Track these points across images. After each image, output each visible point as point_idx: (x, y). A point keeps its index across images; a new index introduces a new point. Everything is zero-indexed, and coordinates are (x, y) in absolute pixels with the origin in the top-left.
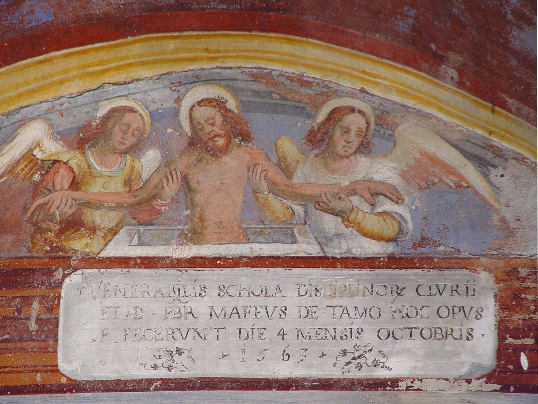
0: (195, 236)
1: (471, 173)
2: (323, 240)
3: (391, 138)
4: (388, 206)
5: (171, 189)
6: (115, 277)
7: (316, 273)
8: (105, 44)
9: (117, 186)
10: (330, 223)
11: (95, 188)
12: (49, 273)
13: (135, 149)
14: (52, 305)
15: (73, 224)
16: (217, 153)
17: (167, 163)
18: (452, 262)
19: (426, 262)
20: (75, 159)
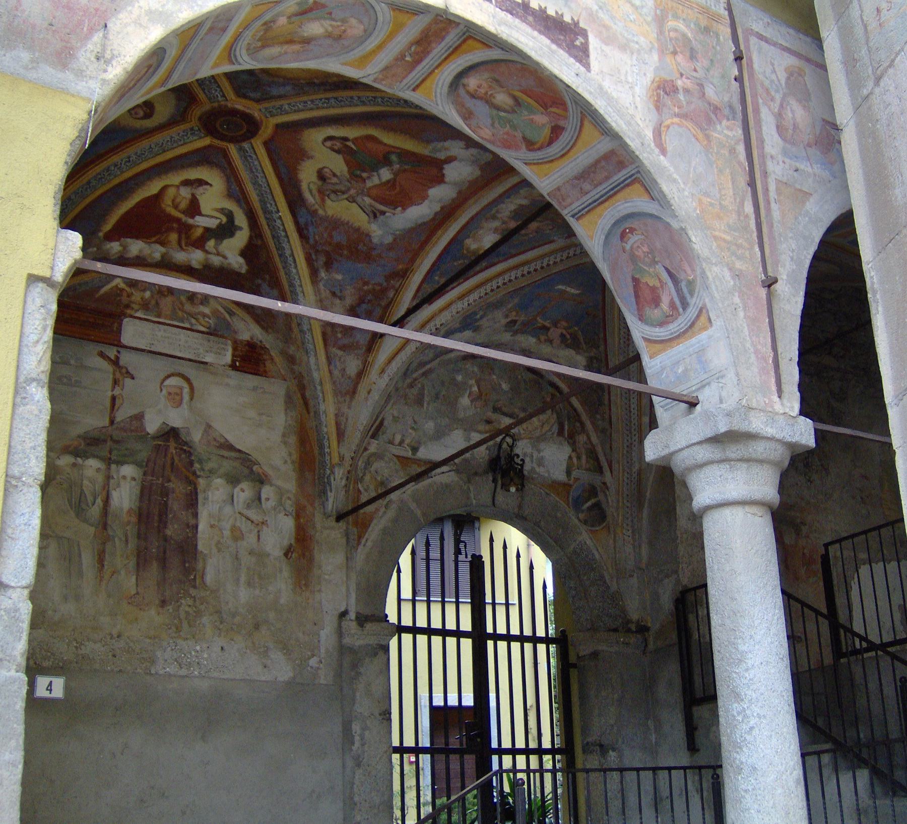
0: (159, 316)
1: (227, 316)
2: (191, 324)
3: (208, 302)
4: (207, 319)
5: (153, 302)
6: (137, 321)
7: (189, 332)
8: (282, 273)
9: (139, 299)
10: (193, 321)
11: (133, 298)
12: (120, 316)
13: (144, 290)
14: (120, 325)
15: (128, 306)
16: (165, 296)
17: (152, 296)
18: (222, 336)
19: (216, 335)
20: (128, 289)
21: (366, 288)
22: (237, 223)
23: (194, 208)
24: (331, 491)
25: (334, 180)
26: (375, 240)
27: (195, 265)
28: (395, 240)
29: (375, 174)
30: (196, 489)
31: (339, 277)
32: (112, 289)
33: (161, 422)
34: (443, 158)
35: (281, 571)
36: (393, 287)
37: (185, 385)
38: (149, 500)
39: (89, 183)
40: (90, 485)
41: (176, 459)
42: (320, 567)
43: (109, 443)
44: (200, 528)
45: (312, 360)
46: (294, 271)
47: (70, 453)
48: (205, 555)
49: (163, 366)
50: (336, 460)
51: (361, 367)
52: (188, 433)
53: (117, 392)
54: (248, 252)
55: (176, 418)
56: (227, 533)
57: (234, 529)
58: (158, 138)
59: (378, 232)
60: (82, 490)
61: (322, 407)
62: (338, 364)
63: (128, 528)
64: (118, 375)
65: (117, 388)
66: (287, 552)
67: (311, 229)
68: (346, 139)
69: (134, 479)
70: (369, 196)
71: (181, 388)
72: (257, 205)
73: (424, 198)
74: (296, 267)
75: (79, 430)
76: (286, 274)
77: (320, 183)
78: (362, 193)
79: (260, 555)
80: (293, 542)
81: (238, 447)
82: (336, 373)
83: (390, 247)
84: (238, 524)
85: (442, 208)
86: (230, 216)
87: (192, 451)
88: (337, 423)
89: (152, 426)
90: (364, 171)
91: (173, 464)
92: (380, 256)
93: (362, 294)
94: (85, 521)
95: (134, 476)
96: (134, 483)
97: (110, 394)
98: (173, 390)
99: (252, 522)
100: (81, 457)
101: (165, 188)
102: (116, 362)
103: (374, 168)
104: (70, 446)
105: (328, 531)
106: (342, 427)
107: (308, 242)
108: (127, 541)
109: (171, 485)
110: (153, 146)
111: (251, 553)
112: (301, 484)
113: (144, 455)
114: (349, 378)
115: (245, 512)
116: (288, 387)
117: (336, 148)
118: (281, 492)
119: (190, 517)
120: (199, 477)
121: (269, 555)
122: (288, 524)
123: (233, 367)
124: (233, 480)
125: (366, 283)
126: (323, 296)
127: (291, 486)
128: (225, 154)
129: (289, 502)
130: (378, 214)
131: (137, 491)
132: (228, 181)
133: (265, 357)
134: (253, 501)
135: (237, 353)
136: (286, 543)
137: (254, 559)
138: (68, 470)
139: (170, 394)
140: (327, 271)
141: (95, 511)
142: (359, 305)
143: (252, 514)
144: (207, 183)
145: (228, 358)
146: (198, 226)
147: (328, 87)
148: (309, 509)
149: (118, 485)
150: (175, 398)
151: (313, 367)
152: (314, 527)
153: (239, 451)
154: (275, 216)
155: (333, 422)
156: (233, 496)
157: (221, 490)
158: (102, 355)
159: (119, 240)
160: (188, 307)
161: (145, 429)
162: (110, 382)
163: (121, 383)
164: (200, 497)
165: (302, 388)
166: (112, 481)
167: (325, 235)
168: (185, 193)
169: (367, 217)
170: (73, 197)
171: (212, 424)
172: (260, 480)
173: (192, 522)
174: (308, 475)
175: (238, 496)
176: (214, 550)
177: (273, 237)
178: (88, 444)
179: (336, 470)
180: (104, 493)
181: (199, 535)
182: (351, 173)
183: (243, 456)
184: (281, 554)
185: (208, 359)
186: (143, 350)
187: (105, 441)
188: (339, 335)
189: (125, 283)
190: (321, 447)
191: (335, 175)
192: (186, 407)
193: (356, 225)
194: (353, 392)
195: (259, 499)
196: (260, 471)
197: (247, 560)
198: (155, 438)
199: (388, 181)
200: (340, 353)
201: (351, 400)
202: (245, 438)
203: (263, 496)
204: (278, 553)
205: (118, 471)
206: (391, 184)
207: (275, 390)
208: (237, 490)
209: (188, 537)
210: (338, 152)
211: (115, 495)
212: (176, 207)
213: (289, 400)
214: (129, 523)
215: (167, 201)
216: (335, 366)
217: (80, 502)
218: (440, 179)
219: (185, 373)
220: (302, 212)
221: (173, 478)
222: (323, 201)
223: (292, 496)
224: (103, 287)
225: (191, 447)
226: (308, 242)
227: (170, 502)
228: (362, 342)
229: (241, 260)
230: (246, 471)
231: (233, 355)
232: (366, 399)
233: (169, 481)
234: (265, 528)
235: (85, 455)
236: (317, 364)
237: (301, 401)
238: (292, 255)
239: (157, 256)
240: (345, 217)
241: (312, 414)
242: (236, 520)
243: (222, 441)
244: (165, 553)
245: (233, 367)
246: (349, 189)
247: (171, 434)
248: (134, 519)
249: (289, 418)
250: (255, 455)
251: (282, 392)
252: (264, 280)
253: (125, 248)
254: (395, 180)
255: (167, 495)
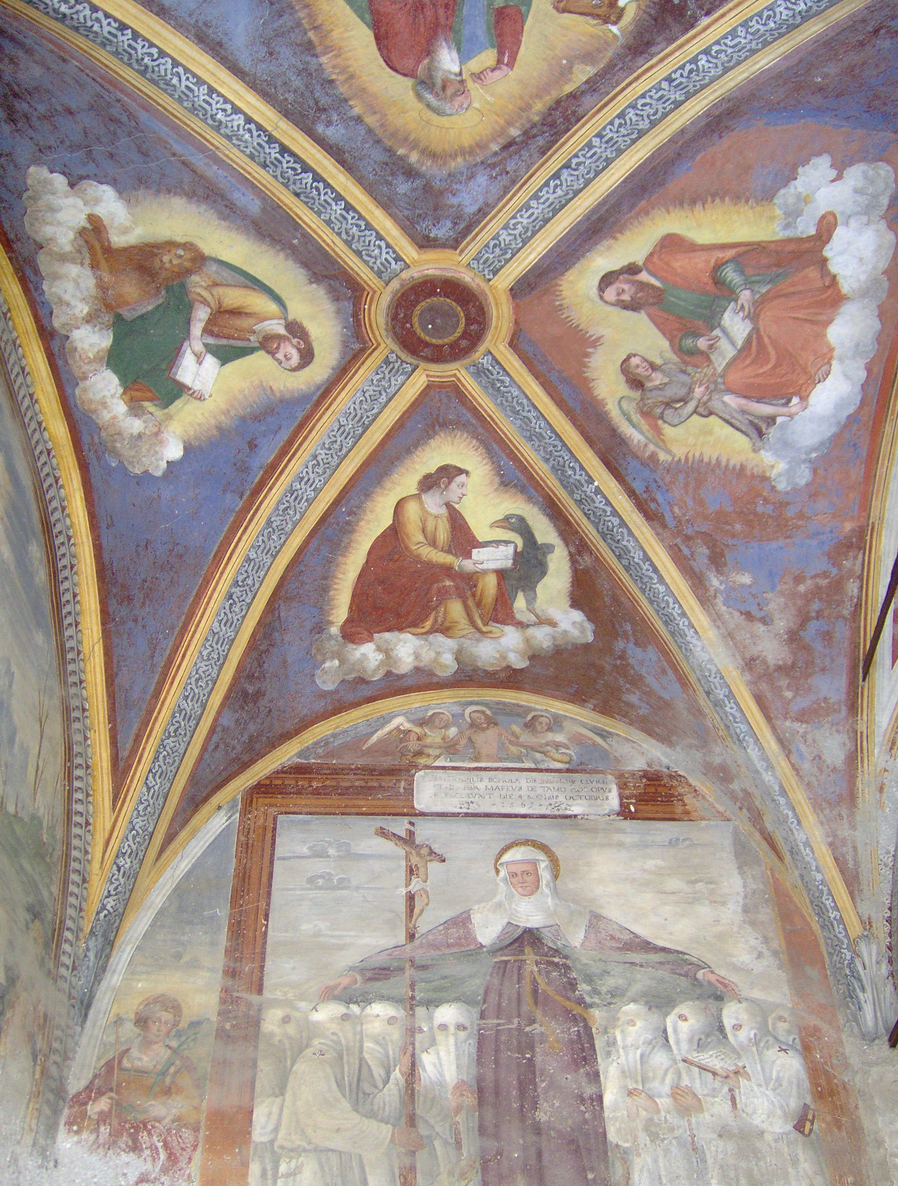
0: (477, 759)
1: (599, 740)
2: (536, 762)
5: (463, 742)
6: (440, 772)
7: (534, 774)
9: (438, 740)
10: (538, 756)
11: (429, 741)
12: (409, 771)
13: (446, 727)
14: (411, 783)
15: (419, 753)
17: (461, 733)
18: (595, 771)
20: (418, 730)
21: (802, 588)
22: (540, 540)
23: (462, 539)
24: (863, 989)
25: (658, 378)
26: (782, 486)
27: (518, 662)
28: (815, 471)
29: (717, 332)
30: (587, 1028)
31: (746, 579)
32: (390, 733)
33: (505, 921)
34: (812, 231)
35: (795, 1162)
36: (851, 573)
37: (541, 856)
38: (496, 1062)
39: (269, 523)
40: (377, 1047)
41: (542, 986)
42: (880, 1143)
43: (409, 972)
44: (608, 1099)
45: (753, 752)
46: (662, 589)
47: (337, 999)
48: (626, 1152)
49: (492, 835)
50: (855, 929)
51: (849, 745)
52: (557, 934)
53: (416, 885)
54: (585, 591)
55: (530, 913)
56: (664, 1102)
57: (677, 1092)
58: (344, 400)
59: (778, 466)
60: (362, 1060)
61: (800, 837)
62: (802, 747)
63: (458, 1119)
64: (415, 860)
65: (414, 880)
66: (801, 1123)
67: (659, 498)
68: (632, 270)
69: (461, 1027)
70: (730, 391)
71: (534, 863)
72: (552, 482)
73: (826, 357)
74: (661, 580)
75: (352, 957)
76: (651, 602)
77: (637, 394)
78: (713, 389)
79: (745, 1139)
80: (808, 1100)
81: (660, 943)
82: (806, 766)
83: (813, 492)
84: (685, 1082)
85: (869, 369)
86: (522, 527)
87: (568, 962)
88: (836, 859)
89: (488, 930)
90: (697, 335)
91: (535, 991)
92: (801, 516)
93: (799, 602)
94: (372, 1115)
95: (461, 1020)
96: (462, 1034)
97: (403, 891)
98: (518, 869)
99: (714, 1074)
100: (356, 1002)
101: (399, 506)
102: (409, 840)
103: (711, 320)
104: (335, 987)
105: (875, 1070)
106: (851, 864)
107: (664, 526)
108: (458, 1144)
109: (537, 1028)
110: (343, 421)
111: (723, 1133)
112: (800, 989)
113: (476, 985)
114: (834, 770)
115: (695, 1056)
116: (736, 833)
117: (626, 297)
118: (761, 1011)
119: (584, 1081)
120: (591, 1006)
121: (762, 1133)
122: (790, 1066)
123: (624, 813)
124: (660, 1002)
125: (798, 579)
126: (732, 625)
127: (778, 994)
128: (456, 391)
129: (782, 1026)
130: (764, 427)
131: (470, 1047)
132: (489, 451)
133: (681, 790)
134: (708, 1035)
135: (627, 792)
136: (794, 1104)
137: (731, 1147)
138: (334, 1027)
139: (514, 875)
140: (719, 572)
141: (390, 1094)
142: (802, 625)
143: (710, 1058)
144: (461, 471)
145: (613, 801)
146: (485, 572)
147: (541, 141)
148: (828, 1034)
149: (433, 1042)
150: (526, 882)
151: (759, 765)
152: (846, 1066)
153: (663, 949)
154: (589, 489)
155: (829, 861)
156: (665, 1031)
157: (639, 1024)
158: (382, 833)
159: (371, 640)
160: (526, 737)
161: (475, 939)
162: (402, 873)
163: (422, 870)
164: (599, 1043)
165: (756, 818)
166: (418, 1037)
167: (690, 503)
168: (433, 503)
169: (747, 439)
170: (253, 555)
171: (605, 913)
172: (716, 995)
173: (589, 1090)
174: (812, 972)
175: (675, 1030)
176: (643, 1138)
177: (604, 536)
178: (370, 979)
179: (863, 948)
180: (406, 1060)
181: (607, 1114)
182: (679, 350)
183: (671, 957)
184: (789, 1127)
185: (576, 810)
186: (455, 815)
187: (401, 969)
188: (789, 694)
189: (409, 721)
190: (821, 911)
191: (653, 367)
192: (547, 891)
193: (735, 461)
194: (852, 797)
195: (721, 1029)
196: (712, 978)
197: (716, 1150)
198: (495, 950)
199: (748, 341)
200: (801, 728)
201: (852, 814)
202: (670, 925)
203: (728, 1022)
204: (780, 1126)
205: (431, 1018)
206: (754, 348)
207: (712, 840)
208: (670, 1021)
209: (586, 1121)
210: (632, 306)
211: (427, 1060)
212: (433, 543)
213: (743, 855)
214: (458, 1110)
215: (415, 538)
216: (801, 756)
217: (359, 1080)
218: (830, 297)
219: (541, 842)
220: (631, 468)
221: (539, 1015)
222: (658, 431)
223: (786, 1015)
224: (373, 733)
225: (566, 957)
226: (664, 526)
227: (539, 1059)
228: (834, 698)
229: (577, 616)
230: (684, 982)
231: (621, 797)
232: (880, 805)
233: (532, 1022)
234: (743, 1081)
235: (365, 1000)
236: (765, 758)
237: (765, 845)
238: (647, 558)
239: (448, 663)
240: (710, 453)
241: (788, 858)
242: (679, 1077)
243: (626, 937)
244: (539, 1155)
245: (624, 813)
246: (691, 390)
247: (527, 939)
248: (470, 1100)
249: (750, 881)
250: (696, 953)
251: (728, 842)
252: (625, 636)
253: (387, 652)
254: (756, 330)
255: (532, 1048)
